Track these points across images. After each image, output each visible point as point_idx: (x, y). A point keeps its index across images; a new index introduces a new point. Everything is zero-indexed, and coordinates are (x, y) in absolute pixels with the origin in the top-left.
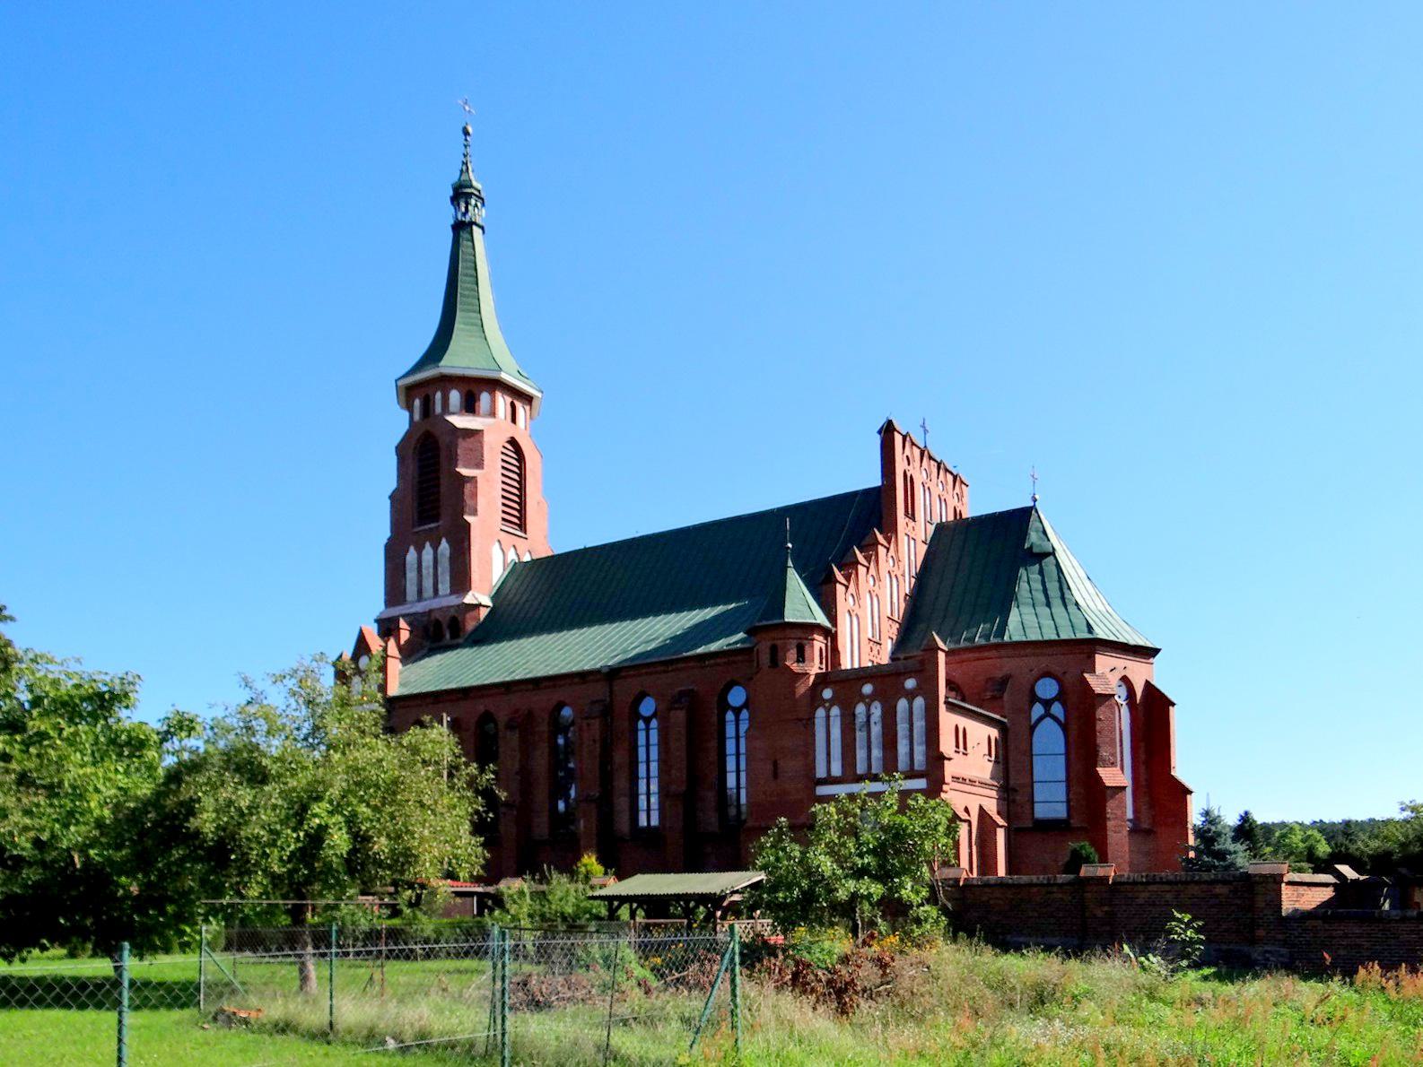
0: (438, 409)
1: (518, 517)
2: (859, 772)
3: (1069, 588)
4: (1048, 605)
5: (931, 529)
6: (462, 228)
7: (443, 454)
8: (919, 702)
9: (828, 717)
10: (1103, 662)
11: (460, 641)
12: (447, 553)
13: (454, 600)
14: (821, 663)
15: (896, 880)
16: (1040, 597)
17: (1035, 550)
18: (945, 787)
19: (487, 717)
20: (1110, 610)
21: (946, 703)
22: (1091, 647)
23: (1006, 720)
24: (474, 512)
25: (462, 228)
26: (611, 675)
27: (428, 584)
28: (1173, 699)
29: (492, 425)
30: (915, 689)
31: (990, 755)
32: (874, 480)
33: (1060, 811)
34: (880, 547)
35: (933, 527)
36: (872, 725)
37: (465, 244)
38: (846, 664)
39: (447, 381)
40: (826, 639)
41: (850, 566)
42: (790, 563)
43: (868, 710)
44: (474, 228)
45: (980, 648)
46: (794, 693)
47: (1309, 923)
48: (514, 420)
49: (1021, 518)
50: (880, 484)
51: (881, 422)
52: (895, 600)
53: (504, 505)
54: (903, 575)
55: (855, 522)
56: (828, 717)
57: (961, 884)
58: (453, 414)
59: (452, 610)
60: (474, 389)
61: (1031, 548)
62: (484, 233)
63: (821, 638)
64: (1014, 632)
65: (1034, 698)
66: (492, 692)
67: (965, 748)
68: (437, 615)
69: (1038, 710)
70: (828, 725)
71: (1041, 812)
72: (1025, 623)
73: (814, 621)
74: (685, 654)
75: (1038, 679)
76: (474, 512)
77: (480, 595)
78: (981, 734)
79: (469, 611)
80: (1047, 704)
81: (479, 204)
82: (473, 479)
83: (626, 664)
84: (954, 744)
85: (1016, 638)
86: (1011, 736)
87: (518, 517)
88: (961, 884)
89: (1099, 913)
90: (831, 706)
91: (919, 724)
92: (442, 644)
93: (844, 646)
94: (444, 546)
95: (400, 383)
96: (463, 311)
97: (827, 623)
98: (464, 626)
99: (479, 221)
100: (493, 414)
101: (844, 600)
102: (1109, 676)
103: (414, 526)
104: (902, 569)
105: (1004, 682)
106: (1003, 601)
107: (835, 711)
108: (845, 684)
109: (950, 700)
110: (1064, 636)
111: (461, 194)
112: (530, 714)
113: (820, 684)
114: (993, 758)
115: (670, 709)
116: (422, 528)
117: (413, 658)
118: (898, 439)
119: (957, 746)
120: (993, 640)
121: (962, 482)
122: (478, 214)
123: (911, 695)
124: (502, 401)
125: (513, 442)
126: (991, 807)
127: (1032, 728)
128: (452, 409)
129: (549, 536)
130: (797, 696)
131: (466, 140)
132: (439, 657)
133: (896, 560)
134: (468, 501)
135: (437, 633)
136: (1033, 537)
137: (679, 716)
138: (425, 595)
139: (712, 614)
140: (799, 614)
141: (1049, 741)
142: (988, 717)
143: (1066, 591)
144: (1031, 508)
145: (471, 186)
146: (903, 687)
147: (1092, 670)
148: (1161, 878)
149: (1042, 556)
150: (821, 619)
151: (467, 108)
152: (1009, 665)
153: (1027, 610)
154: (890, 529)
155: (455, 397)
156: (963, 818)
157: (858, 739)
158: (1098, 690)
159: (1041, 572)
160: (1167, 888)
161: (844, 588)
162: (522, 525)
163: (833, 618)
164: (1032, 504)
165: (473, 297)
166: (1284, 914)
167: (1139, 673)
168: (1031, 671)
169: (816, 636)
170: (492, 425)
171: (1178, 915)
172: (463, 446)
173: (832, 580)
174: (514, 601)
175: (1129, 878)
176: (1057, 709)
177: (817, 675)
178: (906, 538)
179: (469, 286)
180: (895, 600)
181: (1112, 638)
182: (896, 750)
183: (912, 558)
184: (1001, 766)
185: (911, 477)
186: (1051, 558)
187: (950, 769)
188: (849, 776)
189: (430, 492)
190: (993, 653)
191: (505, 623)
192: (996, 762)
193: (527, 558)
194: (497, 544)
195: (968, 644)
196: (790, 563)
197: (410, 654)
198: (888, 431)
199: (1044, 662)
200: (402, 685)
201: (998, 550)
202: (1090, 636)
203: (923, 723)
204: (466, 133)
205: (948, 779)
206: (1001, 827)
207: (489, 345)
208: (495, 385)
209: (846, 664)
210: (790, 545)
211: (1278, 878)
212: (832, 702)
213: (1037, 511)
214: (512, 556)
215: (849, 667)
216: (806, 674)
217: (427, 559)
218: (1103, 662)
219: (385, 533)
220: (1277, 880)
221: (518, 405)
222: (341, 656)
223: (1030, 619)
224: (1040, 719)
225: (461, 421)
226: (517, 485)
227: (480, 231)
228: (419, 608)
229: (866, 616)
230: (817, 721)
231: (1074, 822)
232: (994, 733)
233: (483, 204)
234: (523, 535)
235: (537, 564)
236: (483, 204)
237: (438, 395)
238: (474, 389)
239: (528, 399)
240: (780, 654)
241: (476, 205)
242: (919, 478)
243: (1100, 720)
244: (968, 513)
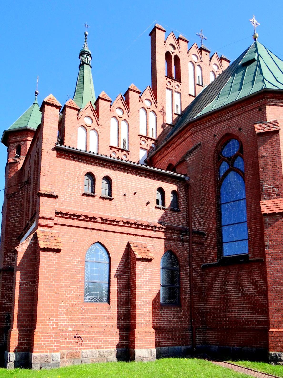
168: (215, 136)
185: (176, 58)
204: (86, 35)
243: (263, 157)
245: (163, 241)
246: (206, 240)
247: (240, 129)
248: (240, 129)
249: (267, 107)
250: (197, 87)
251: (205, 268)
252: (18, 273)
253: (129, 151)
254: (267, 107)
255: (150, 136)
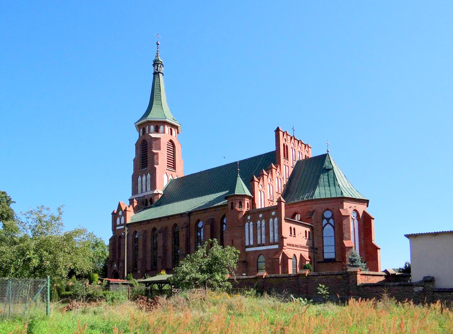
0: (147, 132)
1: (172, 165)
2: (258, 243)
3: (337, 180)
4: (329, 186)
5: (295, 163)
6: (156, 74)
7: (148, 145)
8: (276, 219)
9: (249, 225)
10: (346, 205)
11: (153, 205)
12: (150, 177)
13: (151, 192)
14: (248, 207)
15: (214, 273)
16: (327, 184)
17: (326, 168)
18: (284, 248)
19: (154, 229)
20: (352, 187)
21: (285, 219)
22: (342, 199)
23: (312, 225)
24: (158, 164)
25: (156, 74)
26: (190, 214)
27: (144, 187)
28: (372, 216)
29: (164, 136)
30: (275, 215)
31: (306, 236)
32: (273, 149)
33: (333, 256)
34: (273, 169)
35: (296, 162)
36: (262, 227)
37: (157, 79)
38: (258, 207)
39: (150, 123)
40: (250, 200)
41: (260, 175)
42: (239, 175)
43: (261, 223)
44: (160, 74)
45: (306, 201)
46: (238, 217)
47: (366, 288)
48: (171, 134)
49: (323, 158)
50: (275, 150)
51: (275, 128)
52: (280, 186)
53: (168, 161)
54: (283, 178)
55: (268, 161)
56: (249, 225)
57: (264, 277)
58: (152, 133)
59: (151, 195)
60: (158, 125)
61: (325, 168)
62: (163, 75)
63: (248, 200)
64: (317, 196)
65: (323, 218)
66: (155, 221)
67: (295, 234)
68: (146, 197)
69: (325, 222)
70: (249, 228)
71: (326, 256)
72: (320, 192)
73: (245, 194)
74: (214, 205)
75: (324, 211)
76: (158, 164)
77: (159, 190)
78: (302, 230)
79: (156, 195)
80: (328, 219)
81: (161, 66)
82: (157, 154)
83: (194, 210)
84: (289, 233)
85: (317, 198)
86: (315, 231)
87: (172, 165)
88: (264, 277)
89: (303, 286)
90: (250, 221)
91: (276, 227)
92: (147, 206)
93: (258, 202)
94: (149, 175)
95: (136, 124)
96: (156, 100)
97: (250, 195)
98: (154, 201)
99: (162, 71)
100: (164, 132)
101: (257, 187)
102: (349, 209)
103: (140, 169)
104: (282, 176)
105: (313, 213)
106: (315, 184)
107: (251, 223)
108: (254, 213)
109: (286, 218)
110: (333, 196)
111: (156, 63)
112: (166, 227)
113: (246, 214)
114: (308, 238)
115: (206, 225)
116: (142, 170)
117: (137, 212)
118: (281, 134)
119: (291, 234)
120: (309, 198)
121: (308, 147)
122: (162, 70)
123: (274, 217)
124: (167, 129)
125: (171, 141)
126: (306, 255)
127: (323, 228)
128: (151, 132)
129: (183, 170)
130: (239, 219)
131: (158, 46)
132: (146, 211)
133: (280, 173)
134: (156, 161)
135: (145, 203)
136: (326, 164)
137: (208, 226)
138: (143, 191)
139: (224, 193)
140: (240, 192)
141: (329, 231)
142: (306, 225)
143: (336, 181)
144: (327, 154)
145: (159, 61)
146: (271, 214)
147: (343, 208)
148: (322, 274)
149: (329, 170)
150: (248, 193)
151: (158, 36)
152: (315, 207)
153: (322, 188)
154: (277, 163)
155: (152, 128)
156: (307, 260)
157: (258, 232)
158: (343, 214)
159: (328, 176)
160: (323, 277)
161: (258, 183)
162: (174, 168)
163: (253, 192)
164: (327, 153)
165: (159, 96)
166: (358, 285)
167: (361, 208)
168: (322, 208)
169: (246, 199)
170: (164, 136)
171: (320, 285)
172: (154, 143)
173: (253, 180)
174: (170, 192)
175: (312, 274)
176: (331, 221)
177: (246, 212)
178: (285, 166)
179: (158, 92)
180: (280, 186)
181: (350, 196)
182: (269, 236)
183: (287, 172)
184: (311, 241)
185: (287, 145)
186: (332, 170)
187: (286, 242)
188: (256, 245)
189: (145, 159)
190: (310, 203)
191: (168, 198)
192: (309, 239)
193: (176, 178)
194: (165, 174)
195: (302, 200)
196: (239, 175)
197: (137, 210)
198: (278, 130)
199: (326, 206)
200: (131, 220)
201: (316, 168)
202: (342, 196)
203: (277, 226)
204: (158, 44)
205: (285, 244)
206: (308, 261)
207: (165, 111)
208: (165, 123)
209: (258, 207)
210: (239, 169)
211: (356, 273)
212: (250, 220)
213: (328, 155)
214: (170, 177)
215: (260, 207)
216: (242, 211)
217: (144, 179)
218: (346, 205)
219: (132, 172)
220: (355, 273)
221: (173, 129)
222: (114, 211)
223: (323, 191)
224: (326, 224)
225: (153, 135)
226: (172, 155)
227: (162, 75)
228: (141, 195)
229: (268, 191)
230: (246, 226)
231: (337, 260)
232: (308, 230)
233: (163, 66)
234: (175, 171)
235: (179, 179)
236: (163, 66)
237: (147, 127)
238: (158, 125)
239: (176, 127)
240: (234, 205)
241: (160, 67)
242: (290, 146)
243: (344, 224)
244: (310, 156)
245: (326, 256)
246: (318, 252)
247: (333, 209)
248: (333, 209)
249: (344, 203)
250: (294, 161)
251: (318, 262)
252: (280, 266)
253: (273, 201)
254: (344, 203)
255: (279, 192)
